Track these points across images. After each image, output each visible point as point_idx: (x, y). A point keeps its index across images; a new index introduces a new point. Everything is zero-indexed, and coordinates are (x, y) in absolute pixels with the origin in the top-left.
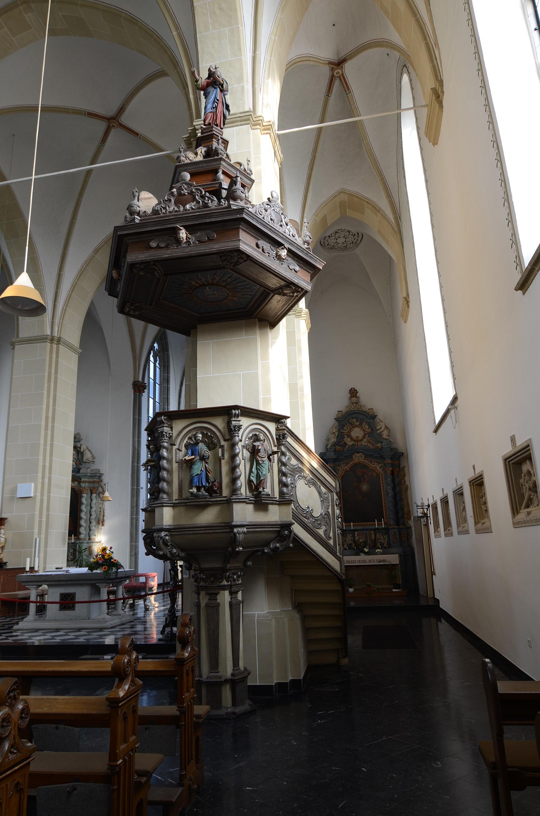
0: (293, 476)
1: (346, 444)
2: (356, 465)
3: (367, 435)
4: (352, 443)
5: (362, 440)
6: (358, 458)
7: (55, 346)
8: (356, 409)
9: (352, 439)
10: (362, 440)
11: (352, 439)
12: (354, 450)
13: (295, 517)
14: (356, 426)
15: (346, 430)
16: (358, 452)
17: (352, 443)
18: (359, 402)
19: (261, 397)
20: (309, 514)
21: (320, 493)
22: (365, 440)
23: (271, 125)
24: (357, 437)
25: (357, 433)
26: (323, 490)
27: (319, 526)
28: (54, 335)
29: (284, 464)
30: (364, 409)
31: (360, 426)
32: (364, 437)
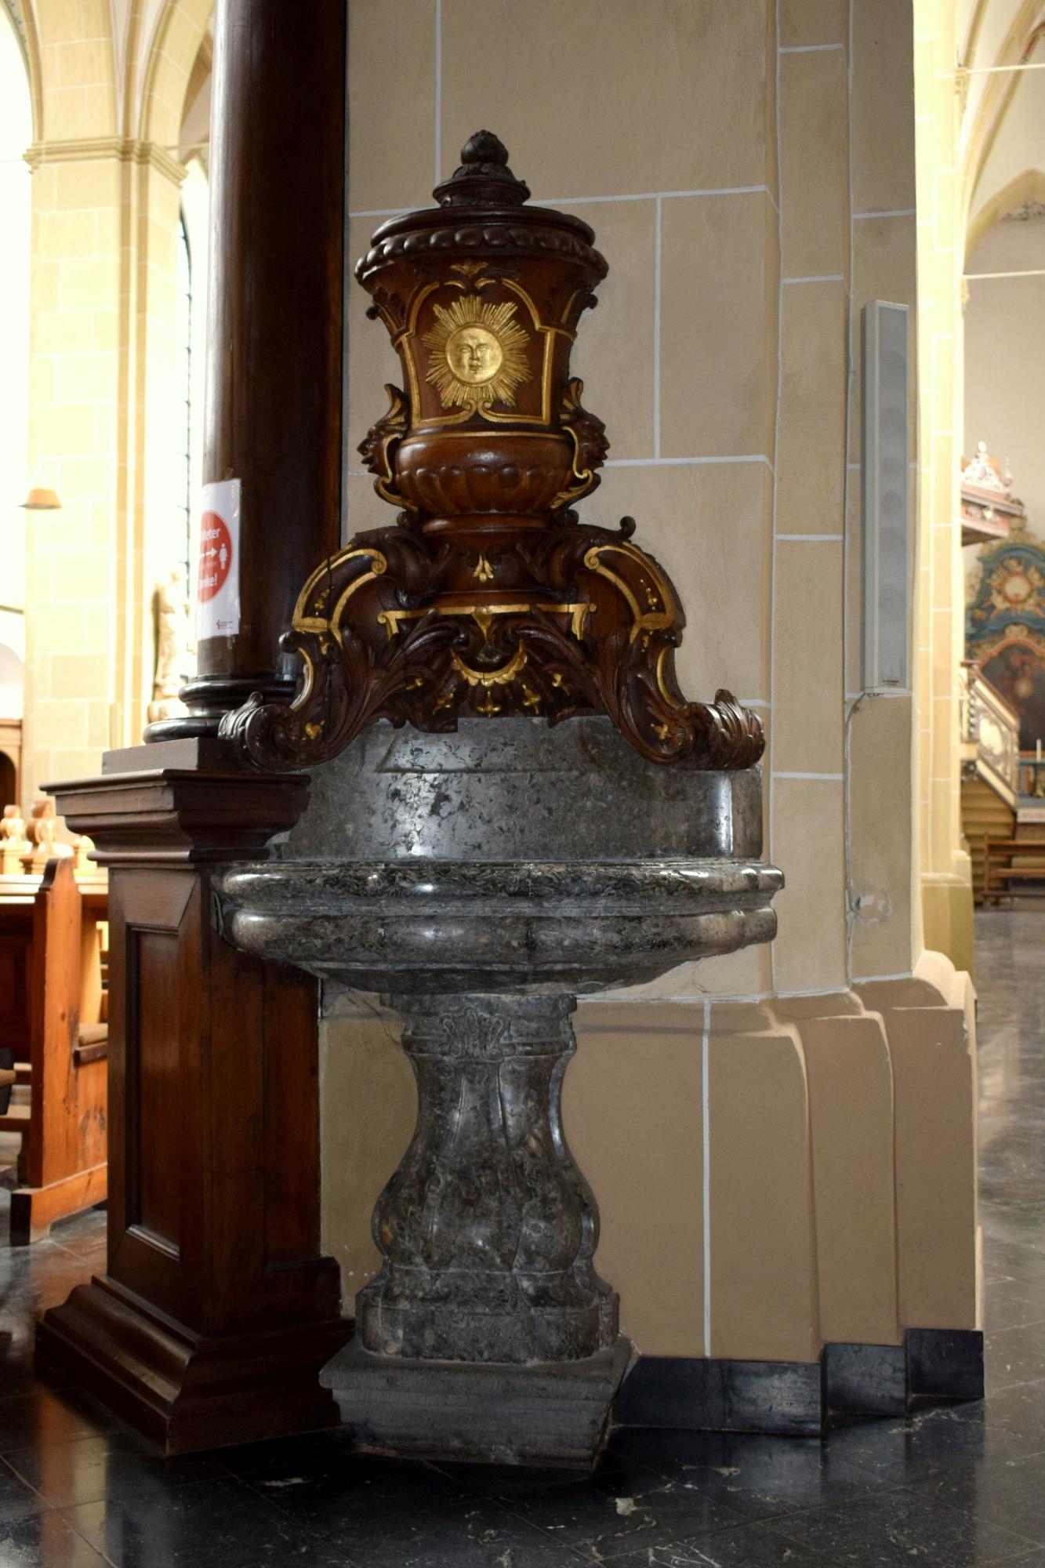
0: (978, 716)
1: (993, 607)
2: (1009, 648)
3: (1035, 593)
4: (1007, 605)
5: (1024, 601)
6: (1016, 634)
7: (134, 167)
8: (1018, 541)
9: (1006, 598)
10: (1024, 601)
11: (1006, 598)
12: (1009, 620)
13: (981, 757)
14: (1017, 574)
15: (995, 581)
16: (1016, 624)
17: (1007, 605)
18: (1025, 526)
19: (932, 610)
20: (990, 752)
21: (1001, 731)
22: (1031, 601)
23: (963, 77)
24: (1017, 595)
25: (1017, 587)
26: (1004, 729)
27: (998, 763)
28: (130, 139)
29: (972, 706)
30: (1033, 542)
31: (1024, 574)
32: (1029, 596)
